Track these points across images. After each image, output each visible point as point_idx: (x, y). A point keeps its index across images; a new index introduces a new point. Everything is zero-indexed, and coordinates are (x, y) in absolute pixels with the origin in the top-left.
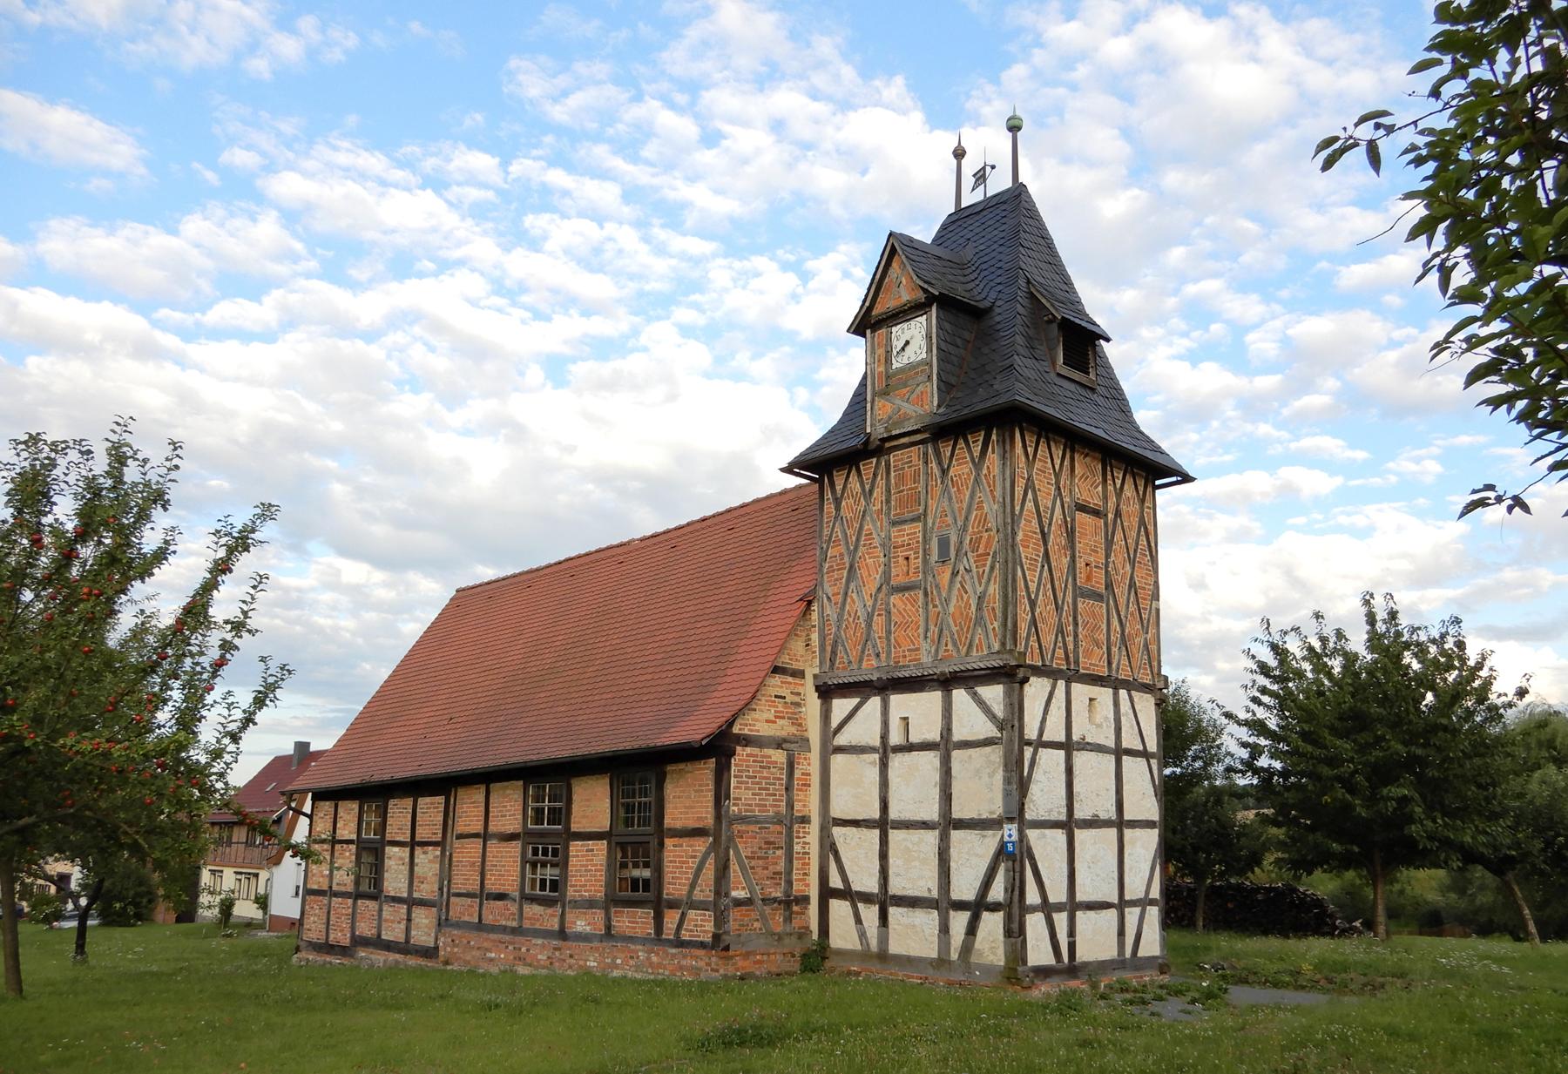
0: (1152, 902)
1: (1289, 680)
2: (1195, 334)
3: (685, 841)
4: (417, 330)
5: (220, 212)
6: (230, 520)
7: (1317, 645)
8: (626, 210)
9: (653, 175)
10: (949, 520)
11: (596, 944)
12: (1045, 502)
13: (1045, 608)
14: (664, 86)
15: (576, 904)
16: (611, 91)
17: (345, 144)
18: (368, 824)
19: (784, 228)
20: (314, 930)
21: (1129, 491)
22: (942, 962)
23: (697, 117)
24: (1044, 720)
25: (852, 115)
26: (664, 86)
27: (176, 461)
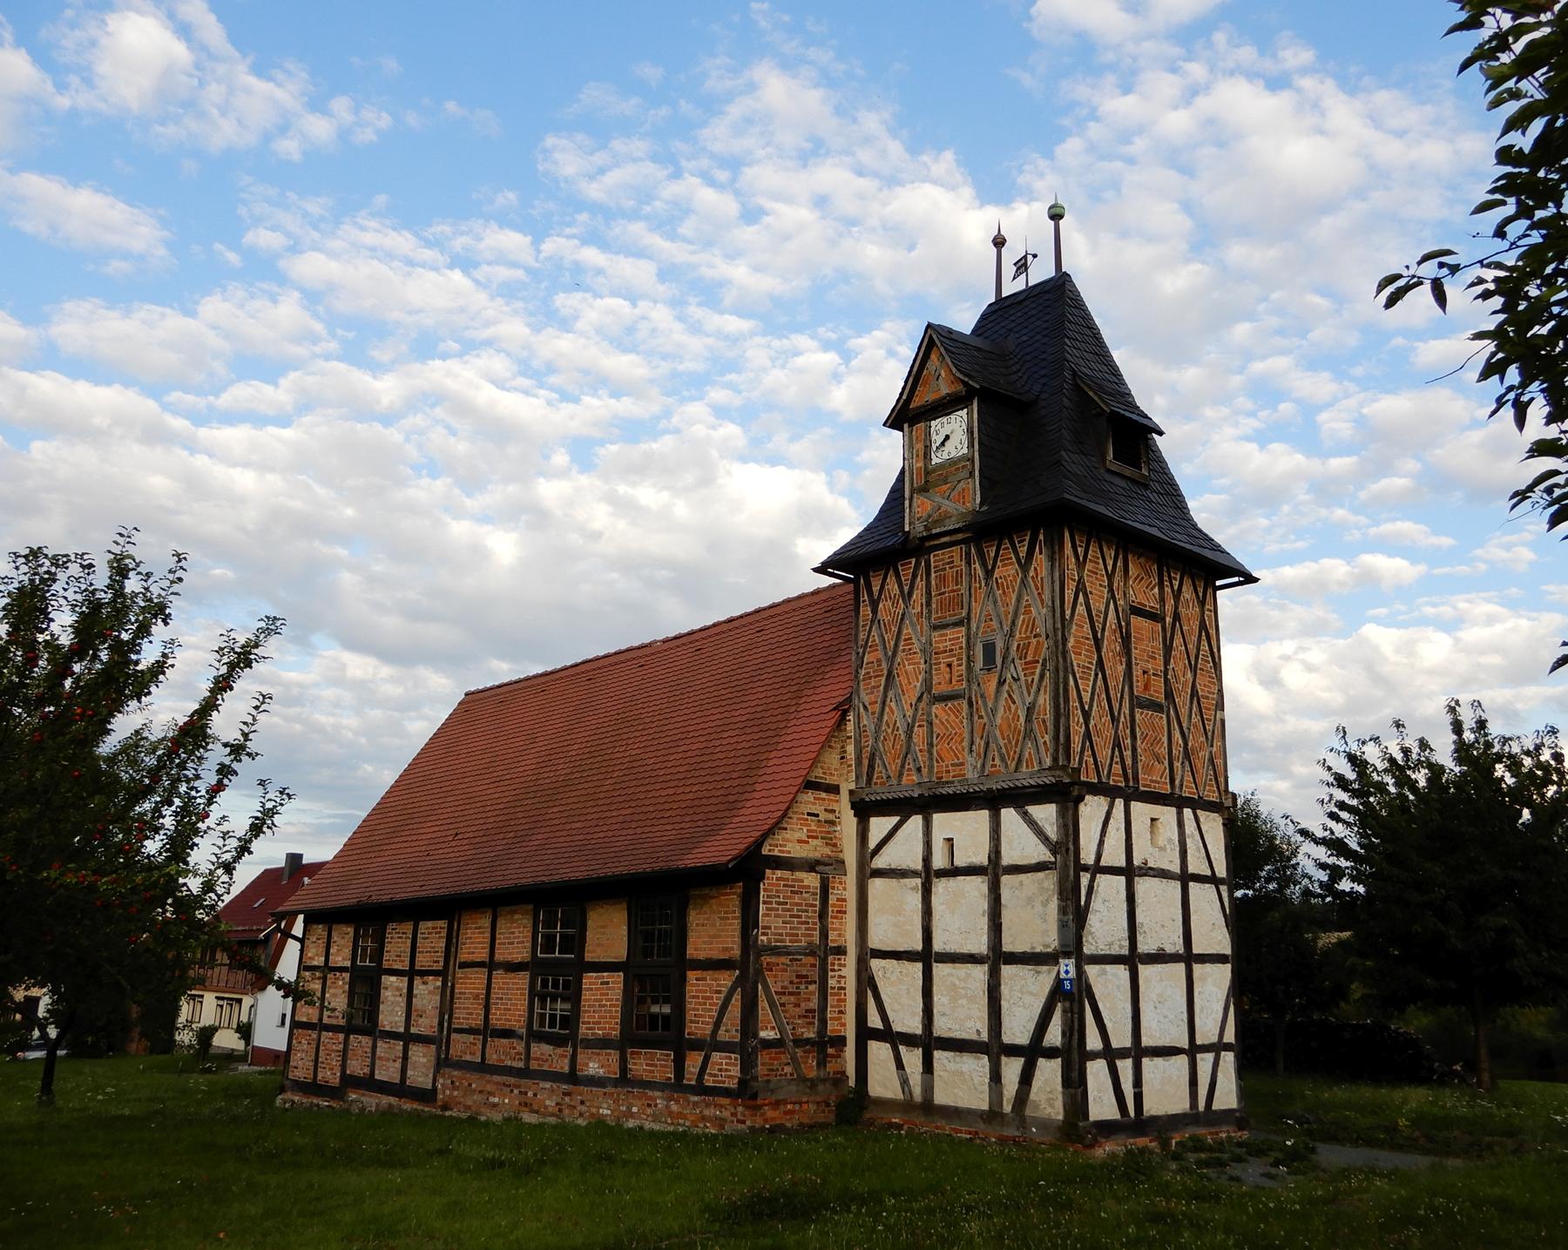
0: (1228, 1047)
1: (1370, 794)
2: (1263, 414)
3: (708, 975)
4: (439, 412)
5: (240, 294)
6: (233, 635)
7: (1399, 757)
8: (661, 288)
9: (693, 253)
10: (995, 624)
11: (609, 1090)
12: (1098, 605)
13: (1099, 719)
14: (705, 163)
16: (649, 168)
17: (373, 224)
18: (364, 949)
19: (829, 306)
20: (301, 1068)
21: (1187, 593)
22: (993, 1115)
23: (737, 193)
24: (1101, 843)
25: (899, 190)
26: (705, 163)
27: (180, 574)
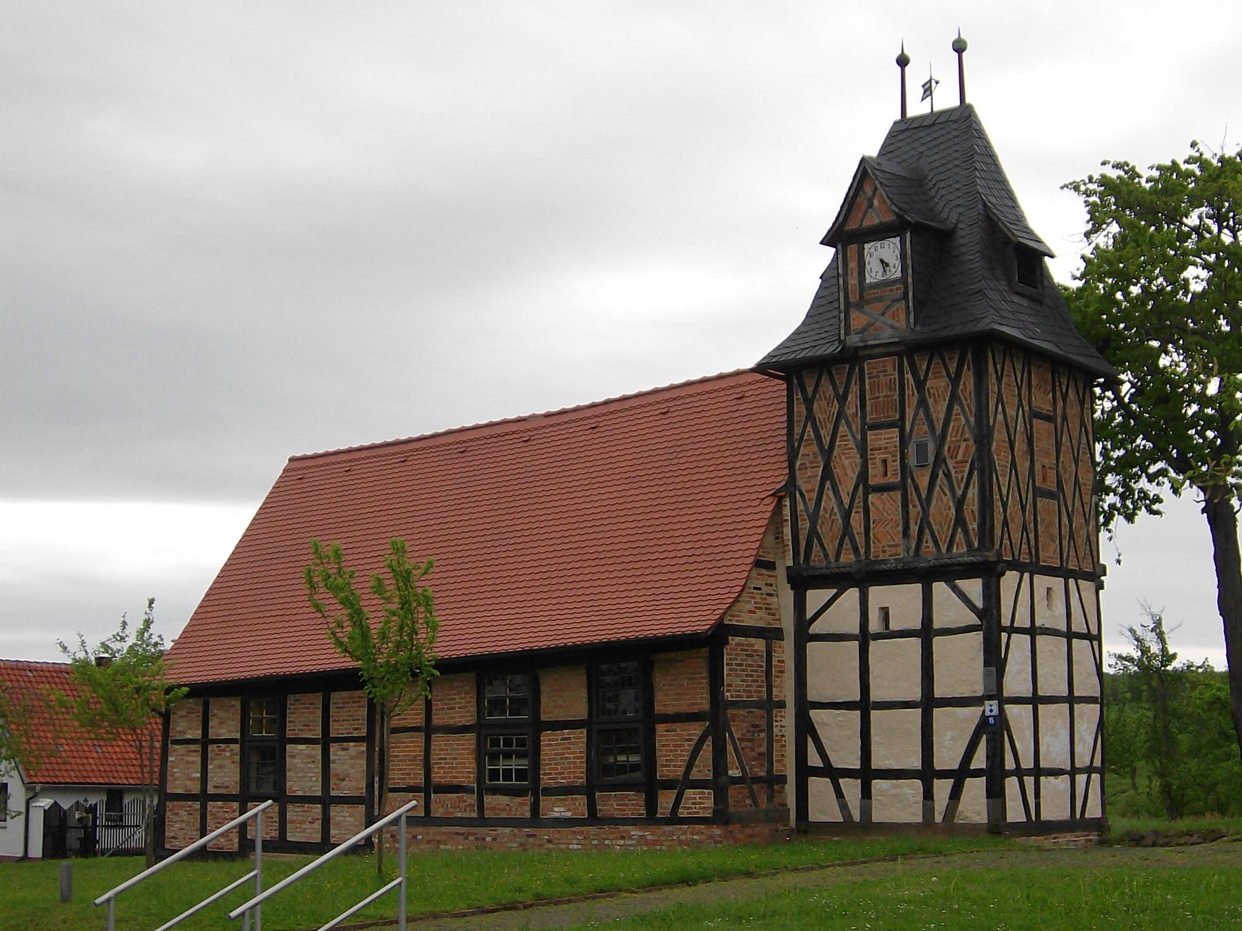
13: (1013, 507)
15: (549, 791)
21: (1072, 395)
